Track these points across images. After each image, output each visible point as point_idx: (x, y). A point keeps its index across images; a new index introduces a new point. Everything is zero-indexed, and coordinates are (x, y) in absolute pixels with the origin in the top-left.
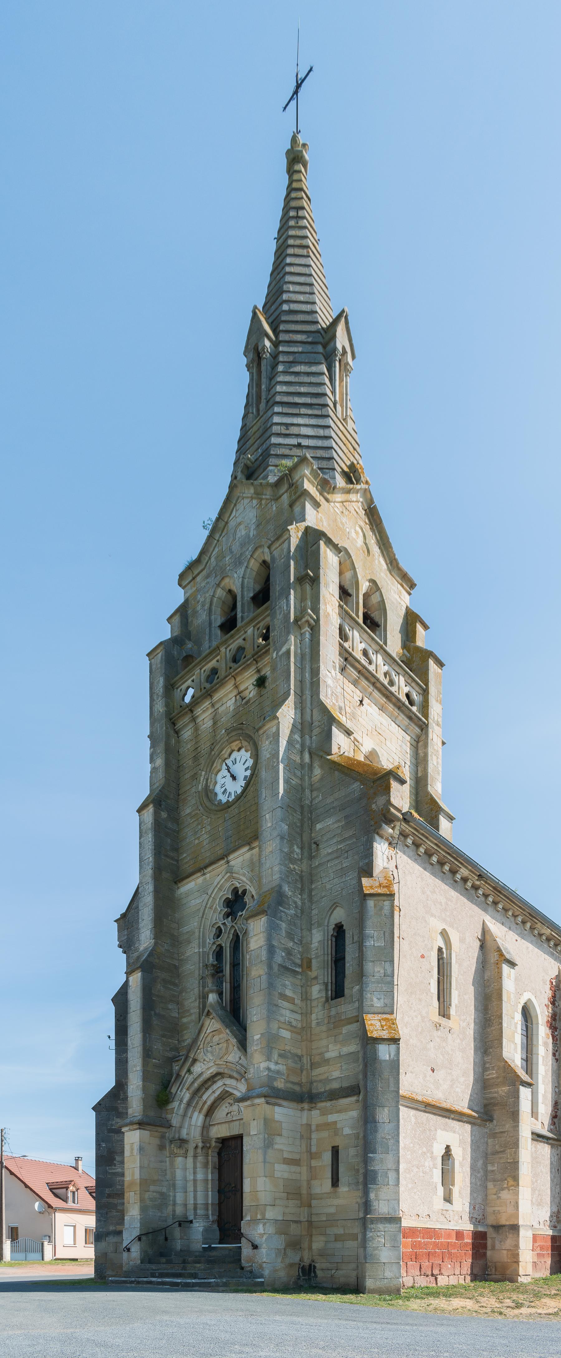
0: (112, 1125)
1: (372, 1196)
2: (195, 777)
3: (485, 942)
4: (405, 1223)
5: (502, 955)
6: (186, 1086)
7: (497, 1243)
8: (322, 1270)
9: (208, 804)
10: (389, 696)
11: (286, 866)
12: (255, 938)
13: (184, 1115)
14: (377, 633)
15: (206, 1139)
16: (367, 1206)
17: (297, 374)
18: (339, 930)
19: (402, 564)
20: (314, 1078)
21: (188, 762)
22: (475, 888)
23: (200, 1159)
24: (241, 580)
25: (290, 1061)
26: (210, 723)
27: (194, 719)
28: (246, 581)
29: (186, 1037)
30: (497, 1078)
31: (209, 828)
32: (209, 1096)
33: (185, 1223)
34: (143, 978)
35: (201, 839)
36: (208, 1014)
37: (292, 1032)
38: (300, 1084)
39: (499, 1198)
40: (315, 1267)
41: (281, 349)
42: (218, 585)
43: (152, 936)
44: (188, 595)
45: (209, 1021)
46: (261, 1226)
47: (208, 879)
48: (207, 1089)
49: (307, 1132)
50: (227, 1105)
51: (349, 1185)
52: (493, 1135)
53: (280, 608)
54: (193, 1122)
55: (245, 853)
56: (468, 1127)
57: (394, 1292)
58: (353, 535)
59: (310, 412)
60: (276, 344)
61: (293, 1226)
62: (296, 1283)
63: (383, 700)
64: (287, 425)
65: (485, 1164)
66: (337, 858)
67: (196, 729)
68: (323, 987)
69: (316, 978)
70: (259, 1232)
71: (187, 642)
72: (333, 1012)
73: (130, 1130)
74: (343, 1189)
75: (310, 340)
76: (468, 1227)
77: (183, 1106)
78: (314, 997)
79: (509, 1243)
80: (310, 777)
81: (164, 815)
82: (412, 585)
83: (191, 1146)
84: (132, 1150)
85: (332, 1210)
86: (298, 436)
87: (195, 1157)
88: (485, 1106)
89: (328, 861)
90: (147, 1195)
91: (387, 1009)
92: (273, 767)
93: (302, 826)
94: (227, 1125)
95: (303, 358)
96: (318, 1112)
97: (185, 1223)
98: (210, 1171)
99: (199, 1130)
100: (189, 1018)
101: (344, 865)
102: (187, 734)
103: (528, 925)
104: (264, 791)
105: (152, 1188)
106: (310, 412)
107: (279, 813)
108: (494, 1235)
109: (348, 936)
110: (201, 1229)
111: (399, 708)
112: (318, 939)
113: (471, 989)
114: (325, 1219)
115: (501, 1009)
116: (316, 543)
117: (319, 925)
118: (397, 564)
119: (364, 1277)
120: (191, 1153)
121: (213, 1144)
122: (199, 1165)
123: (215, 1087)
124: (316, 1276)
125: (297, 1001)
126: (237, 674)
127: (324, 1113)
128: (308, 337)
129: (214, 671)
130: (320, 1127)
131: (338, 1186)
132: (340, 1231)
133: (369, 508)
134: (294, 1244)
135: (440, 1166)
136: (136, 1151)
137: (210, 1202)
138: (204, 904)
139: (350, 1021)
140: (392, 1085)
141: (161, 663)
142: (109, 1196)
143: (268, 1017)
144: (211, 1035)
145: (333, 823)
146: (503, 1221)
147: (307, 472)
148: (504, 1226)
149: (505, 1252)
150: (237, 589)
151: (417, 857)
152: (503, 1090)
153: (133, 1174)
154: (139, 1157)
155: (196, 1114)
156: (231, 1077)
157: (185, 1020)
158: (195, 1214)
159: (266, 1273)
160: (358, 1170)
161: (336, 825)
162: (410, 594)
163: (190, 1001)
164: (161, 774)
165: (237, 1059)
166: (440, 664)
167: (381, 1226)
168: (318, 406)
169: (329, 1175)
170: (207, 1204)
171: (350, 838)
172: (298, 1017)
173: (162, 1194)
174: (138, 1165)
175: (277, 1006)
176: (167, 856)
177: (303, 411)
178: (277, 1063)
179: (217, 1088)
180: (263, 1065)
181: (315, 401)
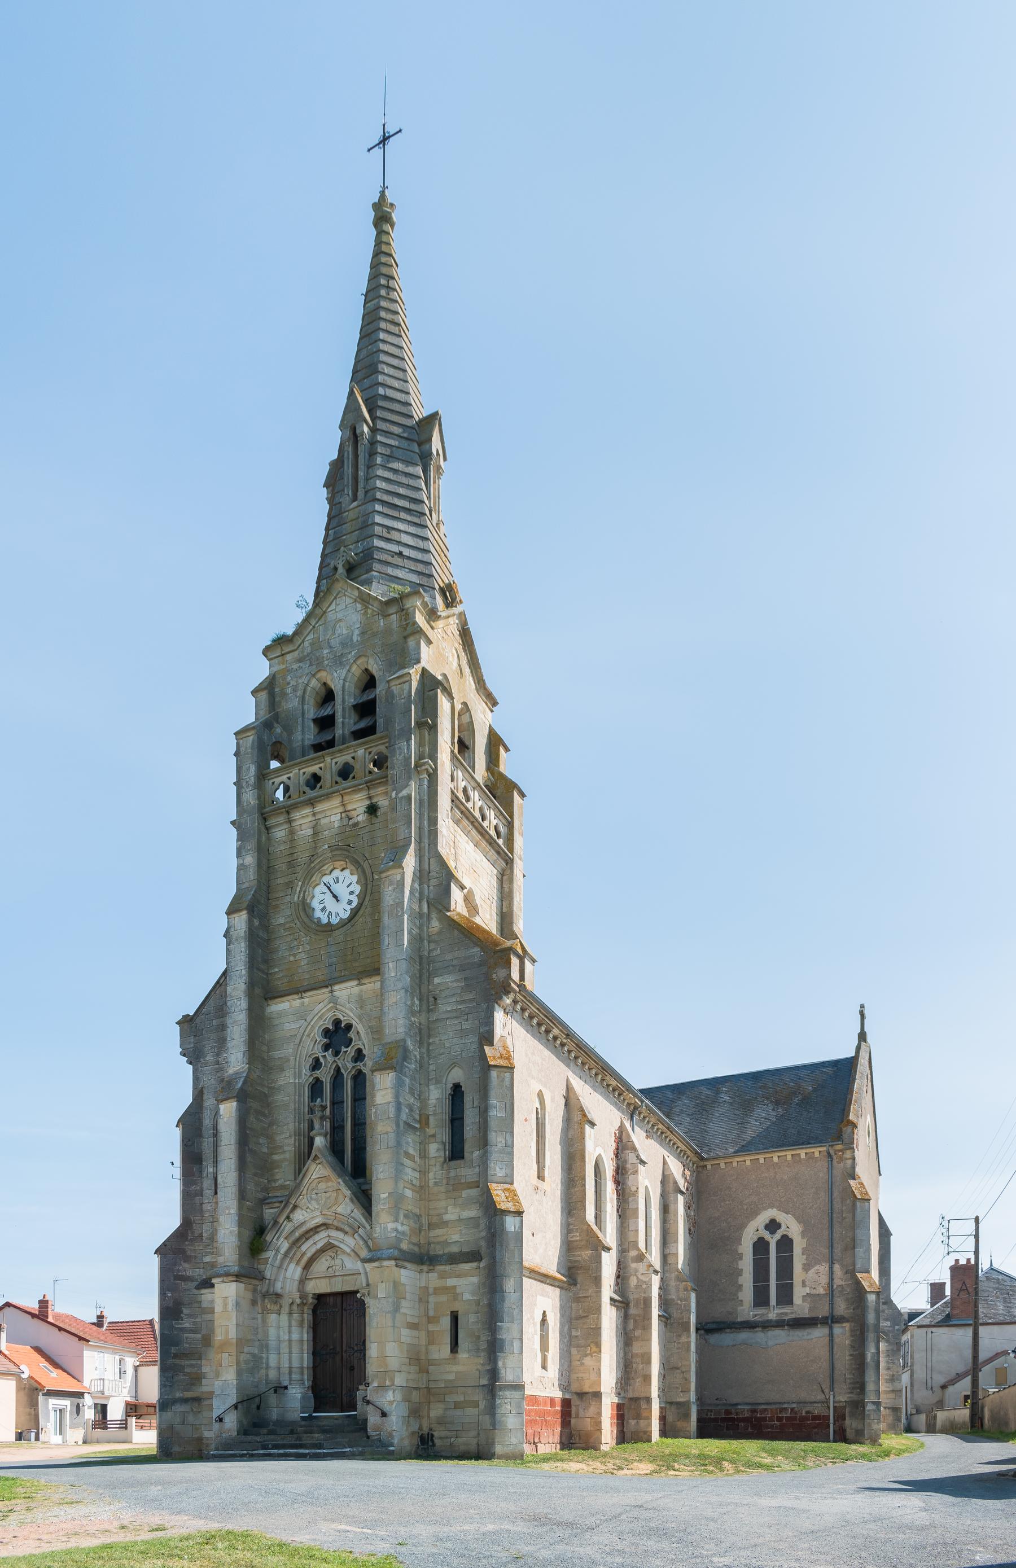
0: (179, 1271)
1: (500, 1364)
2: (290, 885)
3: (570, 1100)
4: (527, 1392)
5: (585, 1115)
6: (284, 1234)
7: (581, 1411)
9: (306, 920)
10: (483, 832)
11: (409, 1019)
12: (382, 1093)
13: (280, 1267)
14: (466, 755)
15: (303, 1296)
16: (494, 1374)
17: (395, 471)
18: (457, 1088)
19: (489, 685)
20: (432, 1240)
21: (281, 866)
22: (563, 1045)
23: (296, 1316)
24: (341, 682)
25: (411, 1222)
26: (310, 832)
27: (290, 822)
28: (347, 684)
30: (581, 1241)
31: (307, 947)
32: (309, 1248)
33: (280, 1389)
34: (239, 1109)
36: (316, 1157)
37: (413, 1191)
38: (419, 1245)
39: (582, 1364)
40: (432, 1436)
41: (379, 438)
42: (314, 675)
43: (246, 1061)
44: (275, 669)
45: (315, 1165)
46: (390, 1393)
47: (307, 1003)
48: (307, 1239)
49: (423, 1296)
50: (328, 1258)
51: (469, 1351)
52: (577, 1299)
53: (400, 748)
54: (289, 1274)
55: (352, 987)
56: (558, 1291)
57: (518, 1457)
58: (451, 659)
59: (409, 518)
60: (374, 430)
61: (415, 1393)
62: (416, 1452)
63: (478, 837)
64: (389, 529)
65: (570, 1329)
67: (292, 832)
68: (441, 1147)
69: (434, 1136)
70: (388, 1399)
71: (276, 725)
72: (452, 1174)
73: (223, 1282)
74: (463, 1355)
75: (405, 435)
76: (558, 1394)
77: (279, 1256)
78: (431, 1156)
79: (592, 1410)
80: (428, 928)
81: (256, 922)
82: (495, 703)
83: (285, 1302)
84: (225, 1305)
85: (452, 1377)
86: (399, 543)
87: (290, 1314)
88: (570, 1269)
90: (243, 1357)
91: (508, 1180)
92: (397, 916)
93: (420, 977)
95: (399, 453)
96: (436, 1274)
97: (280, 1389)
98: (305, 1330)
99: (296, 1283)
100: (282, 1156)
102: (280, 833)
103: (600, 1077)
105: (246, 1349)
106: (409, 518)
107: (404, 965)
108: (578, 1403)
109: (468, 1099)
110: (299, 1396)
111: (490, 844)
112: (436, 1095)
113: (559, 1148)
115: (584, 1171)
116: (434, 689)
117: (438, 1082)
118: (484, 684)
119: (493, 1443)
120: (286, 1309)
121: (310, 1300)
122: (294, 1323)
123: (317, 1237)
124: (434, 1445)
125: (417, 1159)
127: (442, 1276)
128: (404, 432)
129: (316, 778)
130: (437, 1291)
131: (457, 1352)
133: (463, 629)
134: (415, 1413)
135: (539, 1332)
136: (231, 1306)
137: (305, 1365)
138: (302, 1030)
139: (470, 1185)
140: (516, 1256)
141: (252, 748)
143: (396, 1176)
146: (587, 1389)
147: (418, 604)
148: (587, 1393)
149: (588, 1420)
150: (336, 687)
151: (529, 1028)
152: (586, 1254)
153: (227, 1332)
154: (234, 1313)
155: (292, 1266)
156: (338, 1229)
157: (276, 1157)
158: (291, 1380)
159: (396, 1441)
160: (479, 1337)
161: (455, 985)
162: (492, 711)
163: (283, 1136)
164: (251, 874)
165: (349, 1212)
166: (522, 795)
167: (508, 1393)
168: (416, 512)
169: (447, 1339)
170: (302, 1368)
171: (470, 1001)
172: (417, 1175)
173: (253, 1355)
174: (234, 1323)
175: (402, 1164)
176: (258, 969)
177: (403, 515)
178: (403, 1224)
179: (320, 1239)
180: (391, 1226)
181: (413, 507)
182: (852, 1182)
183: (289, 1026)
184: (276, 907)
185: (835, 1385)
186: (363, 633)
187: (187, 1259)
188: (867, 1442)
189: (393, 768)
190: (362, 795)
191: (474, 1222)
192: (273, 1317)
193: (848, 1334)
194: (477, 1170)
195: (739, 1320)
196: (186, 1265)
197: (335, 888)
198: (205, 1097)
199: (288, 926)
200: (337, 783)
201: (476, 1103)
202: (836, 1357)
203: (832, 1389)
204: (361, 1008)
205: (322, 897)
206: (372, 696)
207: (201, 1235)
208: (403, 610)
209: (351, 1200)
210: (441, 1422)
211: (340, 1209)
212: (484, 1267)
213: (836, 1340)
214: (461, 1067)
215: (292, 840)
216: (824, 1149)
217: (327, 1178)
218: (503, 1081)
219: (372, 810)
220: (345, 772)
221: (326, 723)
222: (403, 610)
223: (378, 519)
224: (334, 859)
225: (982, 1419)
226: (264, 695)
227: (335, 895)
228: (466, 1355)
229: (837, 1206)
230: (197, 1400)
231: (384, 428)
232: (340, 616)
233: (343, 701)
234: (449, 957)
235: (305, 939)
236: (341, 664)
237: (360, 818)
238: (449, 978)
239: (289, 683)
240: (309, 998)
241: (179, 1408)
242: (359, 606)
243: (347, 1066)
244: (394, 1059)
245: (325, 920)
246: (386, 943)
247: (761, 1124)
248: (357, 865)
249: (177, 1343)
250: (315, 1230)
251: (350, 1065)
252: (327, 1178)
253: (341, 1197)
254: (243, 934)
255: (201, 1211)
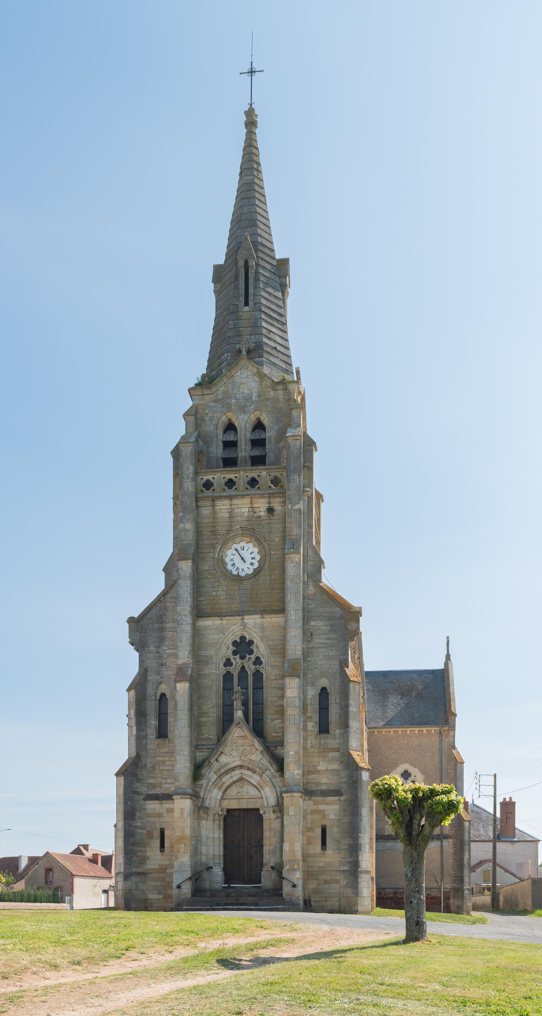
1: (360, 858)
2: (213, 546)
8: (315, 902)
9: (224, 570)
17: (270, 294)
18: (324, 689)
21: (206, 532)
24: (244, 423)
26: (227, 515)
27: (214, 506)
28: (247, 425)
29: (203, 732)
31: (225, 588)
32: (227, 780)
33: (209, 868)
34: (191, 689)
35: (218, 593)
40: (310, 900)
42: (224, 414)
43: (191, 657)
50: (238, 787)
51: (333, 850)
53: (294, 479)
55: (257, 618)
60: (257, 265)
64: (270, 331)
66: (325, 648)
67: (214, 513)
69: (310, 717)
70: (296, 877)
73: (181, 798)
74: (329, 852)
75: (273, 271)
77: (210, 784)
83: (211, 813)
84: (182, 813)
85: (322, 865)
89: (319, 648)
94: (237, 800)
96: (312, 802)
97: (209, 868)
100: (207, 719)
101: (330, 654)
102: (206, 511)
104: (289, 595)
112: (313, 693)
114: (316, 870)
117: (313, 685)
120: (211, 817)
123: (233, 773)
126: (254, 497)
127: (316, 803)
128: (272, 269)
130: (312, 812)
132: (328, 878)
142: (133, 844)
144: (237, 738)
145: (322, 626)
156: (249, 769)
160: (339, 842)
163: (208, 706)
165: (259, 760)
169: (320, 842)
171: (334, 639)
177: (275, 323)
179: (236, 775)
182: (453, 751)
183: (212, 636)
184: (203, 558)
185: (444, 878)
186: (259, 396)
187: (139, 780)
188: (465, 913)
189: (289, 490)
190: (265, 500)
191: (336, 772)
192: (204, 822)
193: (451, 846)
194: (338, 741)
195: (386, 834)
196: (138, 784)
197: (243, 553)
198: (149, 673)
199: (211, 572)
200: (247, 489)
201: (338, 701)
202: (444, 860)
203: (442, 880)
204: (263, 632)
205: (232, 557)
206: (263, 437)
207: (146, 765)
208: (286, 389)
209: (262, 752)
210: (316, 891)
211: (253, 758)
212: (345, 800)
213: (445, 849)
214: (327, 678)
215: (214, 518)
216: (438, 728)
217: (245, 737)
218: (355, 690)
219: (270, 510)
220: (253, 482)
221: (230, 445)
222: (286, 389)
223: (264, 324)
224: (243, 535)
225: (498, 902)
226: (191, 419)
227: (243, 557)
228: (331, 852)
229: (445, 765)
230: (144, 874)
231: (263, 265)
232: (243, 381)
233: (245, 435)
234: (320, 610)
235: (224, 583)
236: (244, 412)
237: (262, 514)
238: (321, 623)
239: (207, 414)
240: (226, 621)
241: (135, 879)
242: (257, 379)
243: (250, 668)
244: (294, 670)
245: (235, 573)
246: (289, 598)
247: (396, 707)
248: (259, 542)
249: (133, 836)
250: (233, 769)
251: (253, 667)
252: (245, 737)
253: (254, 750)
254: (189, 575)
255: (146, 749)
